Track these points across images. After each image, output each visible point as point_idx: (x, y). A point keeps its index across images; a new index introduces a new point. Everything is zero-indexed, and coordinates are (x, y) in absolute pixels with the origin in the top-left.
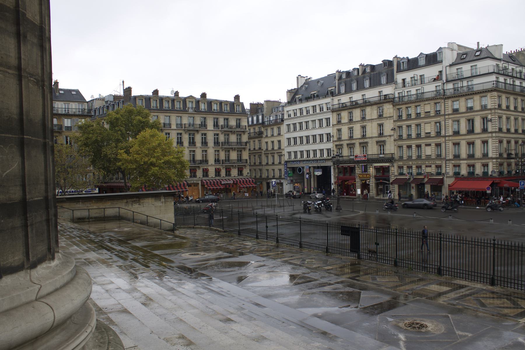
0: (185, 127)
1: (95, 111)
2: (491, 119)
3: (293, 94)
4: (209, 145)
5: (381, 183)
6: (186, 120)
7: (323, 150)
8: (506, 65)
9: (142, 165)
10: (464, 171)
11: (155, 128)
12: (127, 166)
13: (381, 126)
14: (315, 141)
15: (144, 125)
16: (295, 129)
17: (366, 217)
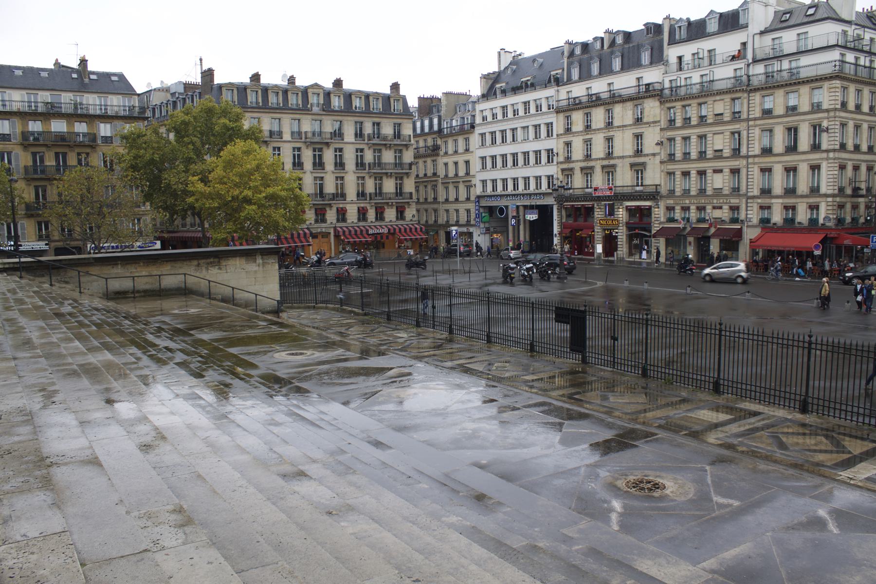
0: (306, 138)
1: (154, 109)
2: (827, 128)
3: (490, 82)
4: (347, 167)
5: (637, 236)
6: (307, 125)
7: (540, 177)
8: (860, 32)
9: (230, 201)
10: (777, 217)
11: (251, 139)
12: (204, 204)
13: (638, 137)
14: (526, 162)
15: (233, 134)
16: (494, 142)
17: (609, 292)
